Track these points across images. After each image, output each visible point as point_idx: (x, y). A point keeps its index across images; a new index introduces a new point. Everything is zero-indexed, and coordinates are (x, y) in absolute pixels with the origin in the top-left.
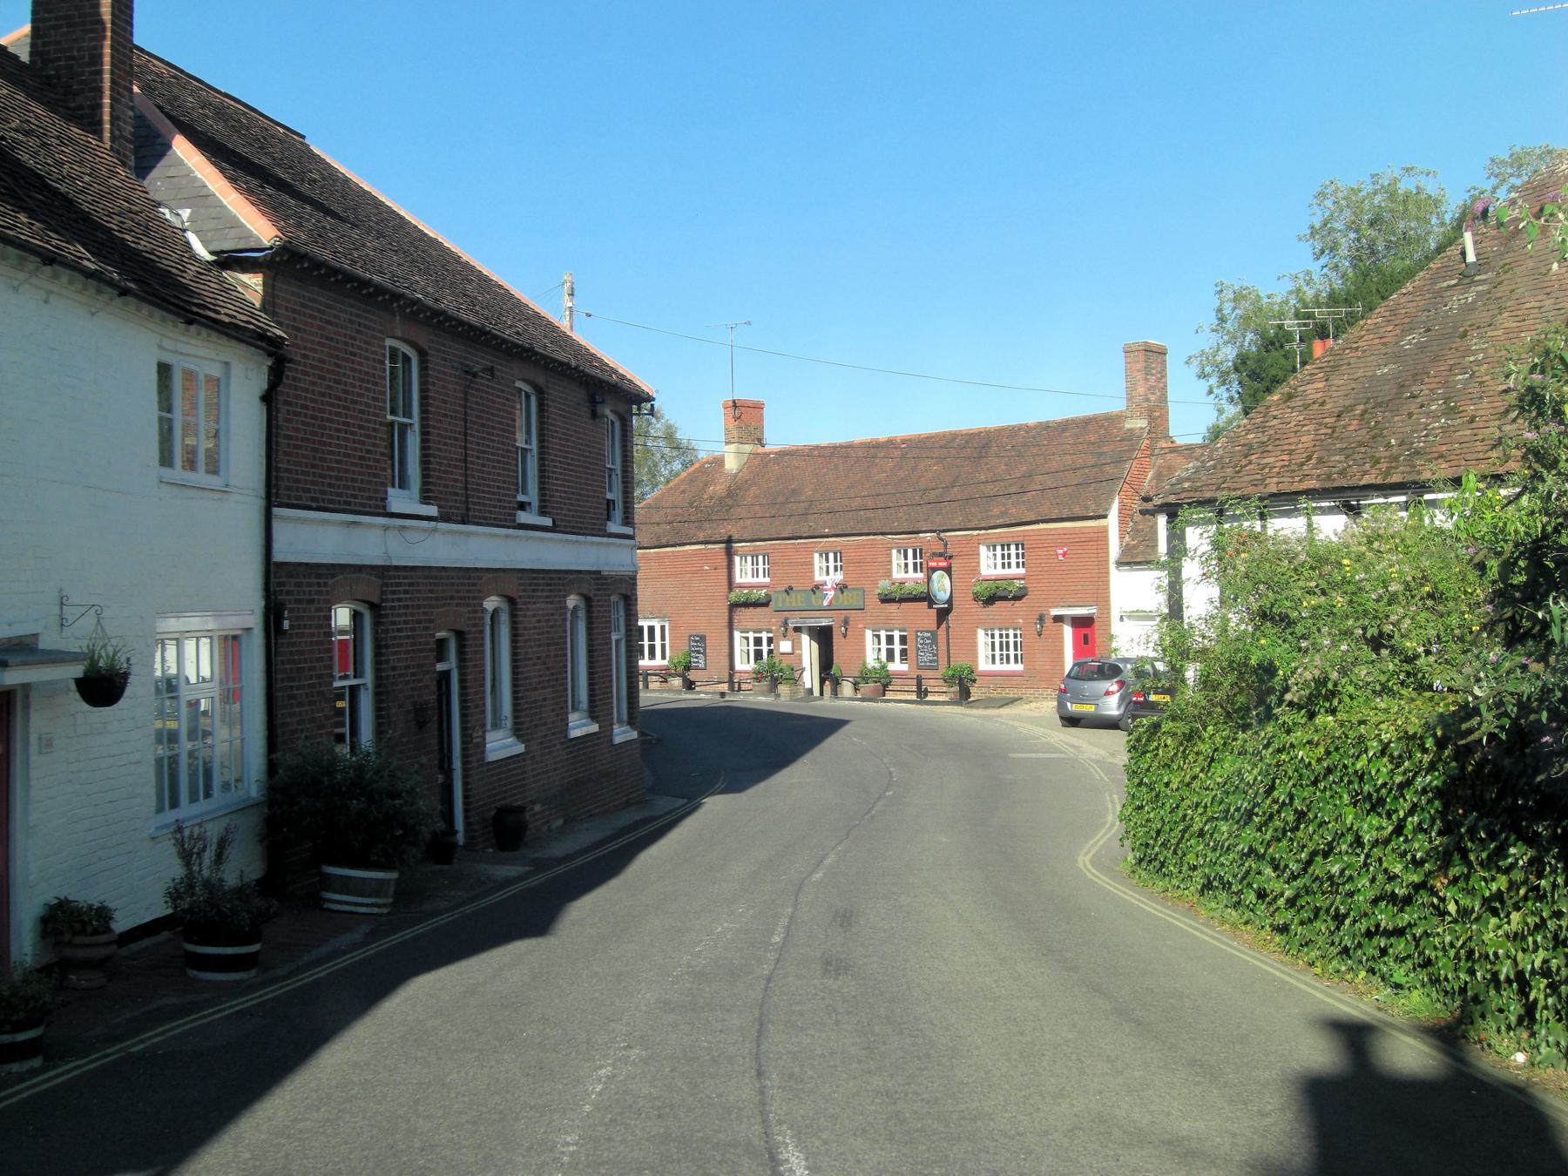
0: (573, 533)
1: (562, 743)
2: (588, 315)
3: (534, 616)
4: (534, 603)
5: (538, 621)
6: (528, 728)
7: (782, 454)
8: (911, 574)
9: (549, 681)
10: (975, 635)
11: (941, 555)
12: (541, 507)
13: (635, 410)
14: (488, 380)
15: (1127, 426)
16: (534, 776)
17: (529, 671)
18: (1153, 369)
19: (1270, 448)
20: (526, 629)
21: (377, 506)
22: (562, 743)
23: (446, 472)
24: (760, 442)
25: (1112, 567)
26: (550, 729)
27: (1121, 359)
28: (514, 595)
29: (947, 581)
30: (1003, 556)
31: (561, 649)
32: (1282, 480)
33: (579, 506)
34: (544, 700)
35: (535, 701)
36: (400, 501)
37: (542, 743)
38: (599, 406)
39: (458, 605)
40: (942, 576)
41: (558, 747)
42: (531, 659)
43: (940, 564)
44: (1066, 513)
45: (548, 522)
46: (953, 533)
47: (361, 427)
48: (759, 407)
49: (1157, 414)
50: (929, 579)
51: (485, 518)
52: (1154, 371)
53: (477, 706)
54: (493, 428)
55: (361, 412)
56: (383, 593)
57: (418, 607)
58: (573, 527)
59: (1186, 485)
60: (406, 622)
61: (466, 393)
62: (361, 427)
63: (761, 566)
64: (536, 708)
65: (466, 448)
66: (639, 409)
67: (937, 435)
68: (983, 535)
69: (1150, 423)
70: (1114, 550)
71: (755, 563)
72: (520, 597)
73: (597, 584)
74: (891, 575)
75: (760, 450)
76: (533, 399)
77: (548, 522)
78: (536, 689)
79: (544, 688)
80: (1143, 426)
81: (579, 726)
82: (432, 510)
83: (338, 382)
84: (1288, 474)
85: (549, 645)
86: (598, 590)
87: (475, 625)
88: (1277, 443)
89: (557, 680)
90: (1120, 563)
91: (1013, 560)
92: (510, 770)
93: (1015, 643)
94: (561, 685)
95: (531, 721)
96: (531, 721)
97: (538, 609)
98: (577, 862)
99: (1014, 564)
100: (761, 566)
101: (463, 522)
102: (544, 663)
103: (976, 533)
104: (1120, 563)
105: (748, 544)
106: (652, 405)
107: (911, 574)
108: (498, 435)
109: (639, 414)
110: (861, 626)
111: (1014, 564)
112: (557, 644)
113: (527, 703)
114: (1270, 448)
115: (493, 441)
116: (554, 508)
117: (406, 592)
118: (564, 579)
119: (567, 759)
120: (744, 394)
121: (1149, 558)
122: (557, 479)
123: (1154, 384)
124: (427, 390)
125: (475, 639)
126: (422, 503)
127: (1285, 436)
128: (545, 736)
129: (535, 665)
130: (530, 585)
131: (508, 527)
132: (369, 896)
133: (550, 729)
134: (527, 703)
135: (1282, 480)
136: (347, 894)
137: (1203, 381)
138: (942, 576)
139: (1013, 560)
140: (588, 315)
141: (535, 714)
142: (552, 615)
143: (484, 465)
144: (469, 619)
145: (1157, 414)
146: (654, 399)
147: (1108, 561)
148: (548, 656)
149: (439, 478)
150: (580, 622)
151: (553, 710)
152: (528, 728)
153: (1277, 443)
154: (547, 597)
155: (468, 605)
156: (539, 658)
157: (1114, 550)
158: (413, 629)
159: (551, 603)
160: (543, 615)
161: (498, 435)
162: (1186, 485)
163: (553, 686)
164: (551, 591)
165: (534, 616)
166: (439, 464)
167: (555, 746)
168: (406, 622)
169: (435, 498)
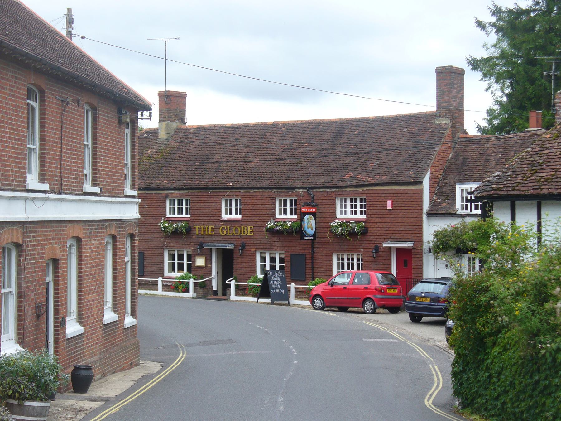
0: (109, 196)
1: (101, 327)
2: (83, 38)
3: (90, 248)
4: (90, 240)
5: (92, 252)
6: (85, 318)
7: (199, 129)
8: (288, 216)
9: (95, 289)
10: (397, 273)
11: (309, 204)
12: (93, 181)
13: (139, 116)
14: (76, 106)
15: (437, 122)
16: (87, 347)
17: (87, 283)
18: (455, 84)
19: (544, 167)
20: (86, 256)
21: (22, 186)
22: (101, 327)
23: (52, 163)
24: (183, 119)
25: (425, 216)
26: (95, 318)
27: (435, 75)
28: (81, 236)
29: (313, 222)
30: (351, 206)
31: (101, 269)
32: (550, 187)
33: (112, 179)
34: (93, 300)
35: (89, 301)
36: (32, 181)
37: (91, 327)
38: (123, 116)
39: (56, 243)
40: (311, 218)
41: (99, 329)
42: (88, 275)
43: (309, 210)
44: (394, 179)
45: (97, 190)
46: (318, 190)
47: (16, 139)
48: (182, 96)
49: (457, 115)
50: (302, 219)
51: (69, 190)
52: (456, 86)
53: (63, 305)
54: (74, 134)
55: (16, 130)
56: (23, 237)
57: (38, 245)
58: (109, 193)
59: (494, 186)
60: (33, 255)
61: (62, 114)
62: (16, 139)
63: (184, 207)
64: (89, 305)
65: (61, 148)
66: (142, 115)
67: (309, 120)
68: (338, 191)
69: (451, 121)
70: (426, 205)
71: (180, 203)
72: (84, 238)
73: (119, 228)
74: (275, 216)
75: (183, 126)
76: (90, 114)
77: (97, 190)
78: (89, 294)
79: (93, 293)
80: (448, 122)
81: (109, 316)
82: (46, 187)
83: (6, 113)
84: (555, 184)
85: (96, 266)
86: (120, 231)
87: (63, 255)
88: (549, 164)
89: (99, 288)
90: (429, 214)
91: (358, 209)
92: (77, 343)
93: (358, 264)
94: (101, 291)
95: (87, 314)
96: (87, 314)
97: (92, 244)
98: (128, 400)
99: (358, 212)
100: (184, 207)
101: (60, 193)
102: (94, 278)
103: (333, 190)
104: (429, 214)
105: (177, 192)
106: (150, 113)
107: (288, 216)
108: (76, 138)
109: (142, 119)
110: (254, 250)
111: (358, 212)
112: (99, 266)
113: (85, 302)
114: (544, 167)
115: (73, 142)
116: (100, 181)
117: (34, 236)
118: (104, 225)
119: (103, 337)
120: (172, 88)
121: (451, 211)
122: (102, 163)
123: (455, 94)
124: (44, 114)
125: (63, 263)
126: (39, 182)
127: (553, 160)
128: (93, 323)
129: (89, 279)
130: (88, 229)
131: (79, 195)
132: (35, 416)
133: (95, 318)
134: (85, 302)
135: (550, 187)
136: (23, 415)
137: (488, 92)
138: (311, 218)
139: (358, 209)
140: (83, 38)
141: (89, 309)
142: (98, 247)
143: (69, 158)
144: (61, 251)
145: (457, 115)
146: (151, 109)
147: (422, 212)
148: (95, 273)
149: (49, 167)
150: (109, 251)
151: (97, 307)
152: (85, 318)
153: (549, 164)
154: (96, 237)
155: (61, 243)
156: (91, 274)
157: (426, 205)
158: (36, 258)
159: (98, 240)
160: (94, 248)
161: (76, 138)
162: (494, 186)
163: (97, 292)
164: (98, 233)
165: (90, 248)
166: (49, 158)
167: (97, 329)
168: (33, 255)
169: (47, 179)
